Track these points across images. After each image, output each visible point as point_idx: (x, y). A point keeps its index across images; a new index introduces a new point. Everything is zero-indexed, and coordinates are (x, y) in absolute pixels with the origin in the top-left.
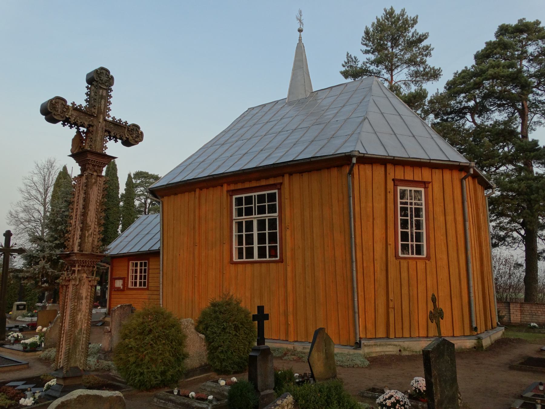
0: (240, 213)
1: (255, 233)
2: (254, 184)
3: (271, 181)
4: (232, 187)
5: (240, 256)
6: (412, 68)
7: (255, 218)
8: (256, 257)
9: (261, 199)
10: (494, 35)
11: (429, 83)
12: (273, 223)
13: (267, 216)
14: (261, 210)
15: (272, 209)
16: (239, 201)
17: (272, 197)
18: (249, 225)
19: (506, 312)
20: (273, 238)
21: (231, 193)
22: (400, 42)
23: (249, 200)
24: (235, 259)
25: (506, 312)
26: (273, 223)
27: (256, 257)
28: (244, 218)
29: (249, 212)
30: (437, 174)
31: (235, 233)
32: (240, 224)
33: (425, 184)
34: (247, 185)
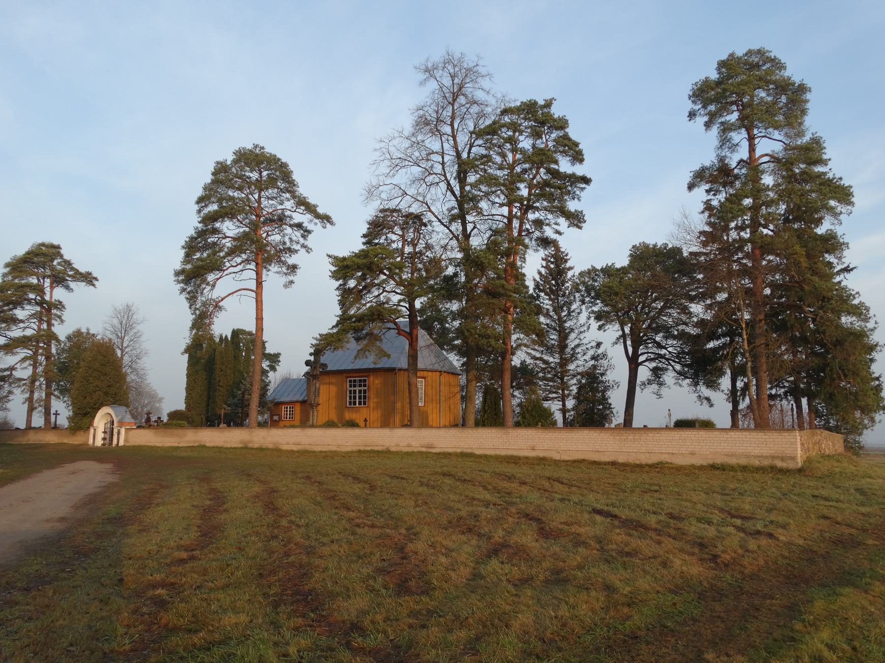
0: (350, 386)
1: (357, 395)
2: (358, 375)
3: (365, 374)
4: (348, 375)
5: (350, 404)
6: (226, 250)
7: (357, 389)
8: (357, 405)
9: (360, 381)
10: (755, 47)
11: (75, 283)
12: (365, 391)
13: (363, 388)
14: (360, 386)
15: (365, 386)
16: (350, 381)
17: (365, 381)
18: (355, 392)
19: (399, 297)
20: (365, 397)
21: (347, 377)
22: (243, 196)
23: (355, 381)
24: (348, 405)
25: (399, 297)
26: (365, 391)
27: (357, 405)
28: (352, 389)
29: (355, 386)
30: (430, 374)
31: (348, 395)
32: (350, 391)
33: (424, 378)
34: (354, 375)
